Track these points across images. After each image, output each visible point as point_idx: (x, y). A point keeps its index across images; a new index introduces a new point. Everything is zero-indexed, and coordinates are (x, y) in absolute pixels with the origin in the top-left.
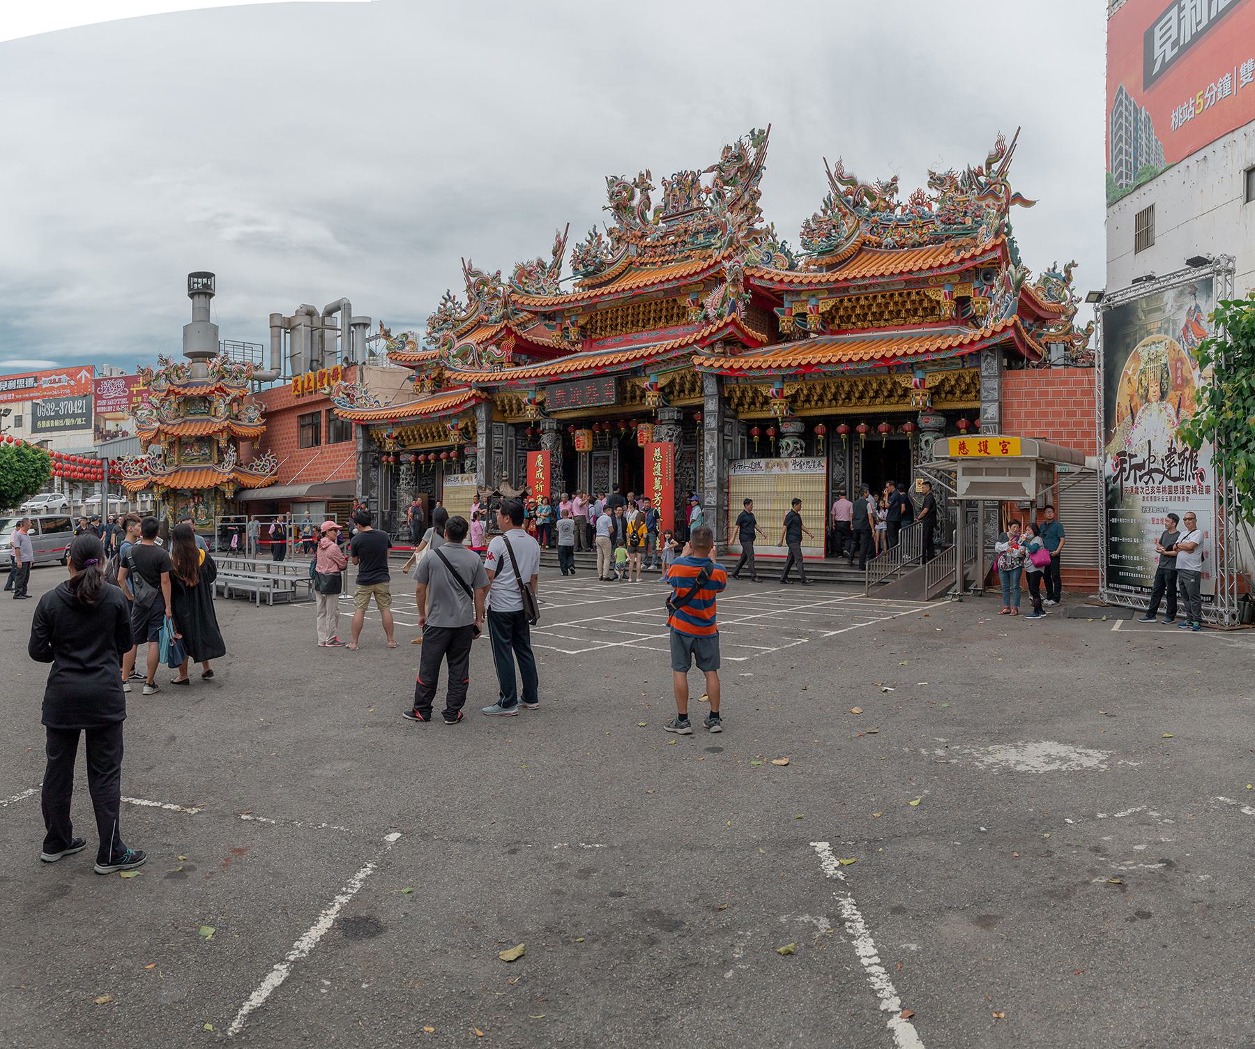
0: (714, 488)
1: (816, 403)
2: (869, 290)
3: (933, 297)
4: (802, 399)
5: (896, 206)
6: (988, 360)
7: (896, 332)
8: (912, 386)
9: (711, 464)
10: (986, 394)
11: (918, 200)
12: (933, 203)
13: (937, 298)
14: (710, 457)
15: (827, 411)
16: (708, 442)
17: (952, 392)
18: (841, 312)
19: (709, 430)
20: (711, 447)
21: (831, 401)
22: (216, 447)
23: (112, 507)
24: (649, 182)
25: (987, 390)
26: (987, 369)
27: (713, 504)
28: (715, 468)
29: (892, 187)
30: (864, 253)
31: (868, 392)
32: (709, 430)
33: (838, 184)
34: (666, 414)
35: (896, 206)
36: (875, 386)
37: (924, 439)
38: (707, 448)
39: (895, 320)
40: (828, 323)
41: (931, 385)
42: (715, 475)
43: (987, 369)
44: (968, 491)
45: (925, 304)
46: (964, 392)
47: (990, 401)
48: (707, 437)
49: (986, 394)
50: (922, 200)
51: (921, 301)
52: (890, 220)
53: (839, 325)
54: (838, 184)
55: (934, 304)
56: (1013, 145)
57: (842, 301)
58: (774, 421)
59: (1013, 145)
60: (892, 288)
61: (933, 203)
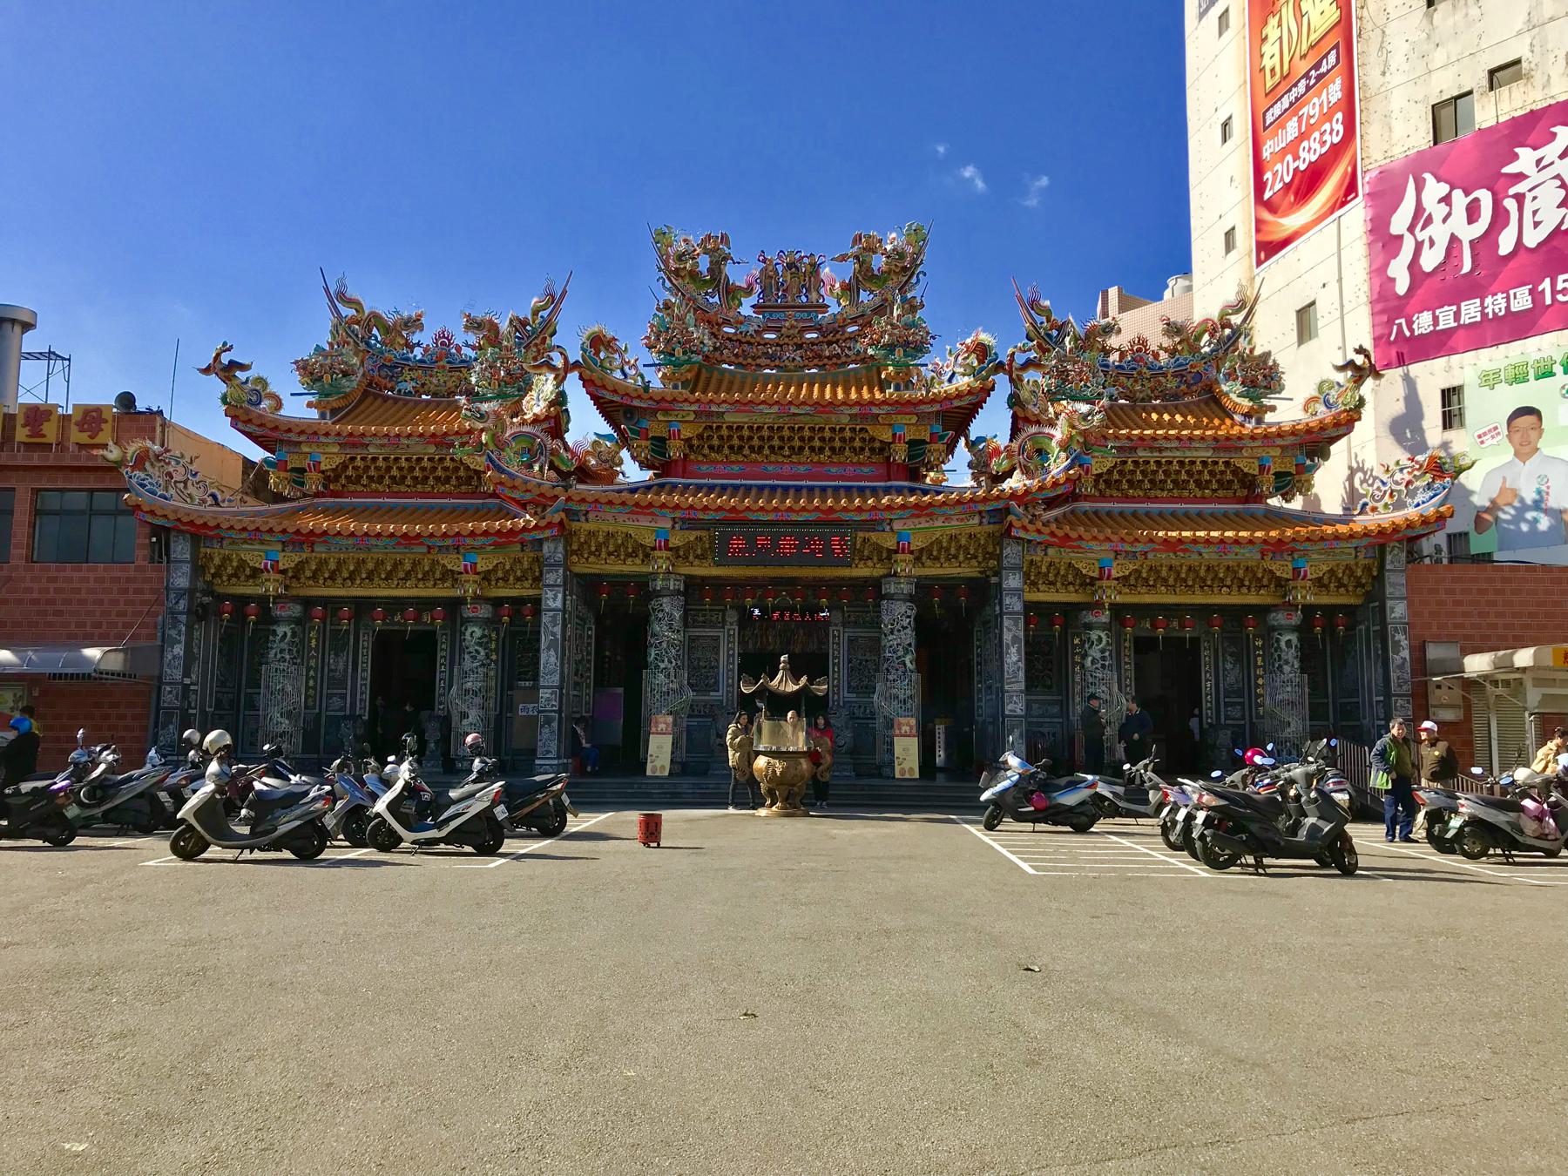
0: (1021, 691)
1: (229, 580)
2: (1164, 454)
3: (472, 466)
4: (212, 571)
5: (415, 345)
6: (1395, 552)
7: (381, 500)
8: (462, 569)
9: (1015, 659)
10: (1391, 590)
11: (444, 339)
12: (1161, 352)
13: (1251, 471)
14: (1013, 650)
15: (357, 592)
16: (1009, 630)
17: (505, 579)
18: (350, 472)
19: (1010, 613)
20: (1014, 637)
21: (345, 579)
22: (1268, 600)
23: (219, 695)
24: (727, 251)
25: (1394, 585)
26: (1392, 562)
27: (1019, 712)
28: (1022, 665)
29: (414, 323)
30: (370, 399)
31: (226, 569)
32: (1010, 613)
33: (339, 306)
34: (672, 582)
35: (415, 345)
36: (217, 561)
37: (470, 630)
38: (1007, 637)
39: (463, 487)
40: (330, 482)
41: (1313, 577)
42: (1021, 675)
43: (1392, 562)
44: (1541, 703)
45: (462, 473)
46: (518, 579)
47: (1397, 598)
48: (1006, 623)
49: (1391, 590)
50: (449, 341)
51: (457, 469)
52: (408, 359)
53: (343, 486)
54: (339, 306)
55: (471, 474)
56: (564, 293)
57: (352, 459)
58: (263, 600)
59: (564, 293)
60: (410, 450)
61: (1161, 352)
